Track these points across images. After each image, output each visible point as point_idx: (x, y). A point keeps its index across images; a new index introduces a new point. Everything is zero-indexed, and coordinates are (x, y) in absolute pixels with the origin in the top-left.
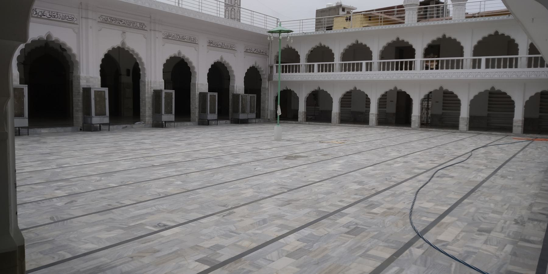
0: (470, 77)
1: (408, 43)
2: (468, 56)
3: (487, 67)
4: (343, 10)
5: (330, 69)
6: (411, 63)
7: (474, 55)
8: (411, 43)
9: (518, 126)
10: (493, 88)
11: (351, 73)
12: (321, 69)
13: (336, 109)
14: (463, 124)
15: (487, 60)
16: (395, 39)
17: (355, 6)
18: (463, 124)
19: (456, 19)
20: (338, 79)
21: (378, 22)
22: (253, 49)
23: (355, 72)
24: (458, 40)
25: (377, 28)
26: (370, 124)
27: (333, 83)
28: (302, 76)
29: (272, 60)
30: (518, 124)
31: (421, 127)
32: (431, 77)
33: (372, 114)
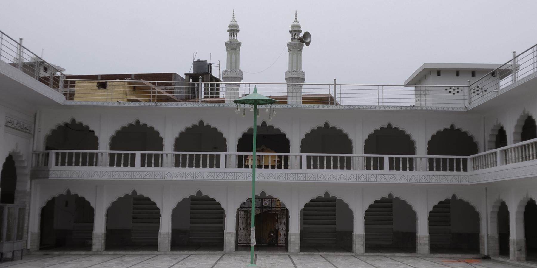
0: (362, 180)
1: (278, 130)
2: (358, 152)
3: (391, 168)
4: (46, 69)
5: (157, 162)
6: (411, 160)
7: (112, 149)
8: (283, 130)
9: (425, 244)
10: (327, 194)
11: (201, 169)
12: (395, 165)
13: (359, 228)
14: (359, 244)
15: (143, 156)
16: (133, 122)
17: (62, 66)
18: (359, 244)
19: (294, 103)
20: (169, 178)
21: (150, 96)
22: (15, 122)
23: (208, 169)
24: (219, 130)
25: (148, 104)
26: (94, 248)
27: (163, 186)
28: (103, 171)
29: (40, 145)
30: (424, 242)
31: (301, 251)
32: (322, 179)
33: (229, 233)
